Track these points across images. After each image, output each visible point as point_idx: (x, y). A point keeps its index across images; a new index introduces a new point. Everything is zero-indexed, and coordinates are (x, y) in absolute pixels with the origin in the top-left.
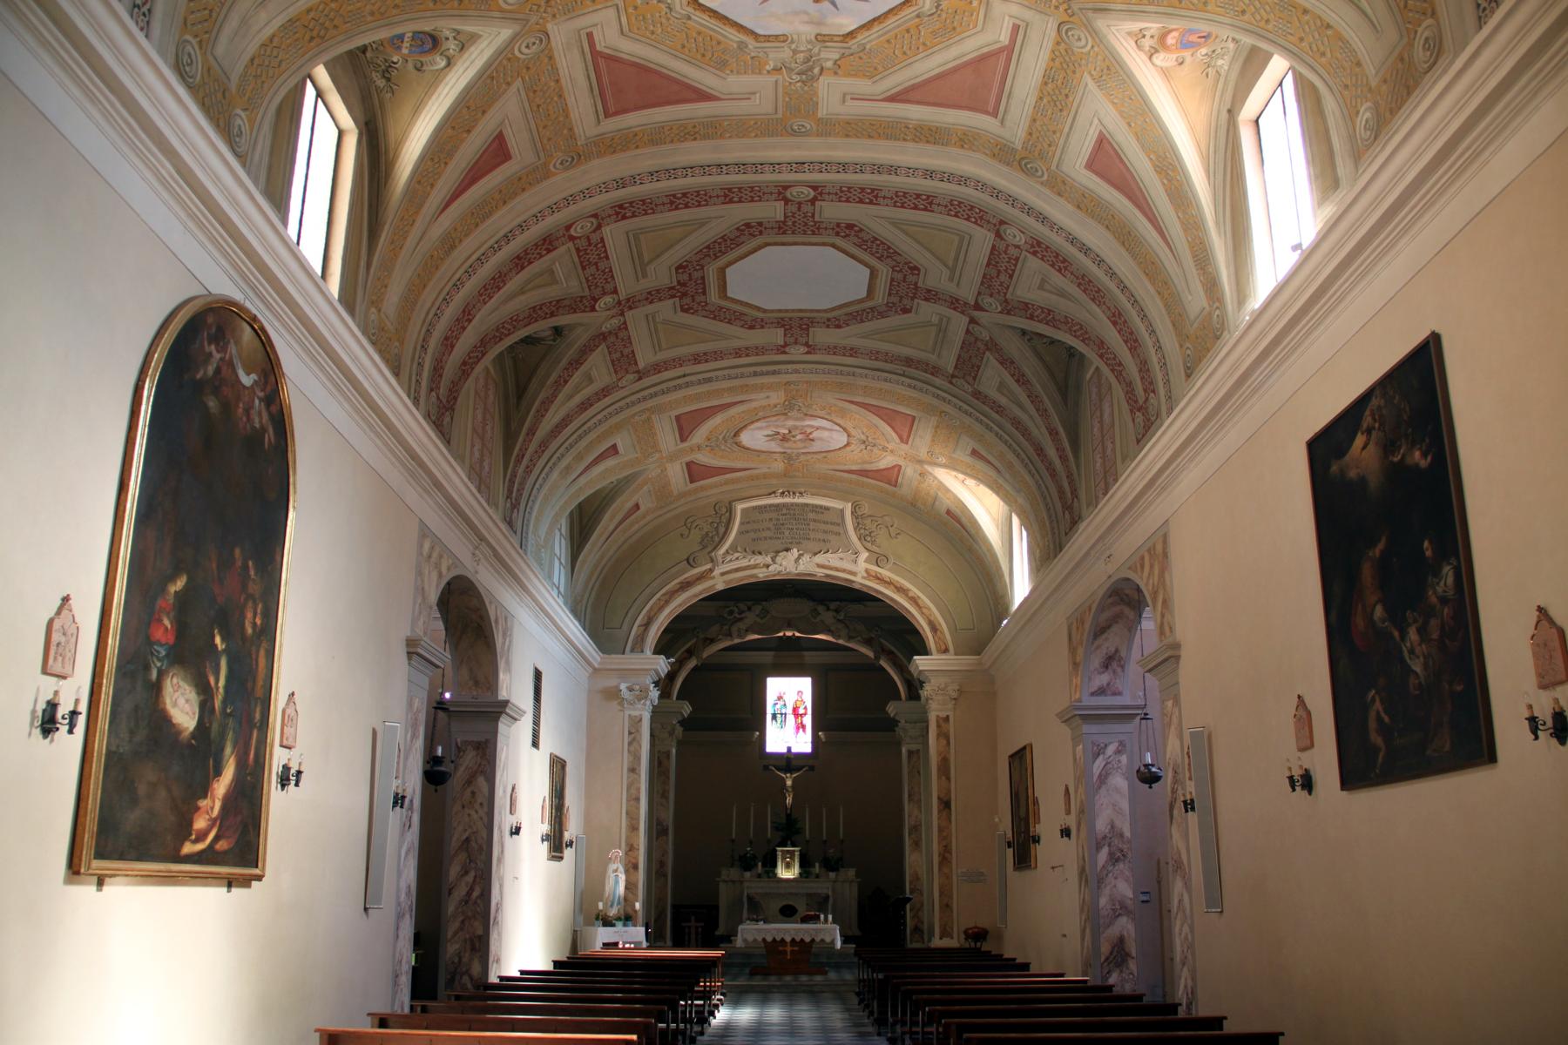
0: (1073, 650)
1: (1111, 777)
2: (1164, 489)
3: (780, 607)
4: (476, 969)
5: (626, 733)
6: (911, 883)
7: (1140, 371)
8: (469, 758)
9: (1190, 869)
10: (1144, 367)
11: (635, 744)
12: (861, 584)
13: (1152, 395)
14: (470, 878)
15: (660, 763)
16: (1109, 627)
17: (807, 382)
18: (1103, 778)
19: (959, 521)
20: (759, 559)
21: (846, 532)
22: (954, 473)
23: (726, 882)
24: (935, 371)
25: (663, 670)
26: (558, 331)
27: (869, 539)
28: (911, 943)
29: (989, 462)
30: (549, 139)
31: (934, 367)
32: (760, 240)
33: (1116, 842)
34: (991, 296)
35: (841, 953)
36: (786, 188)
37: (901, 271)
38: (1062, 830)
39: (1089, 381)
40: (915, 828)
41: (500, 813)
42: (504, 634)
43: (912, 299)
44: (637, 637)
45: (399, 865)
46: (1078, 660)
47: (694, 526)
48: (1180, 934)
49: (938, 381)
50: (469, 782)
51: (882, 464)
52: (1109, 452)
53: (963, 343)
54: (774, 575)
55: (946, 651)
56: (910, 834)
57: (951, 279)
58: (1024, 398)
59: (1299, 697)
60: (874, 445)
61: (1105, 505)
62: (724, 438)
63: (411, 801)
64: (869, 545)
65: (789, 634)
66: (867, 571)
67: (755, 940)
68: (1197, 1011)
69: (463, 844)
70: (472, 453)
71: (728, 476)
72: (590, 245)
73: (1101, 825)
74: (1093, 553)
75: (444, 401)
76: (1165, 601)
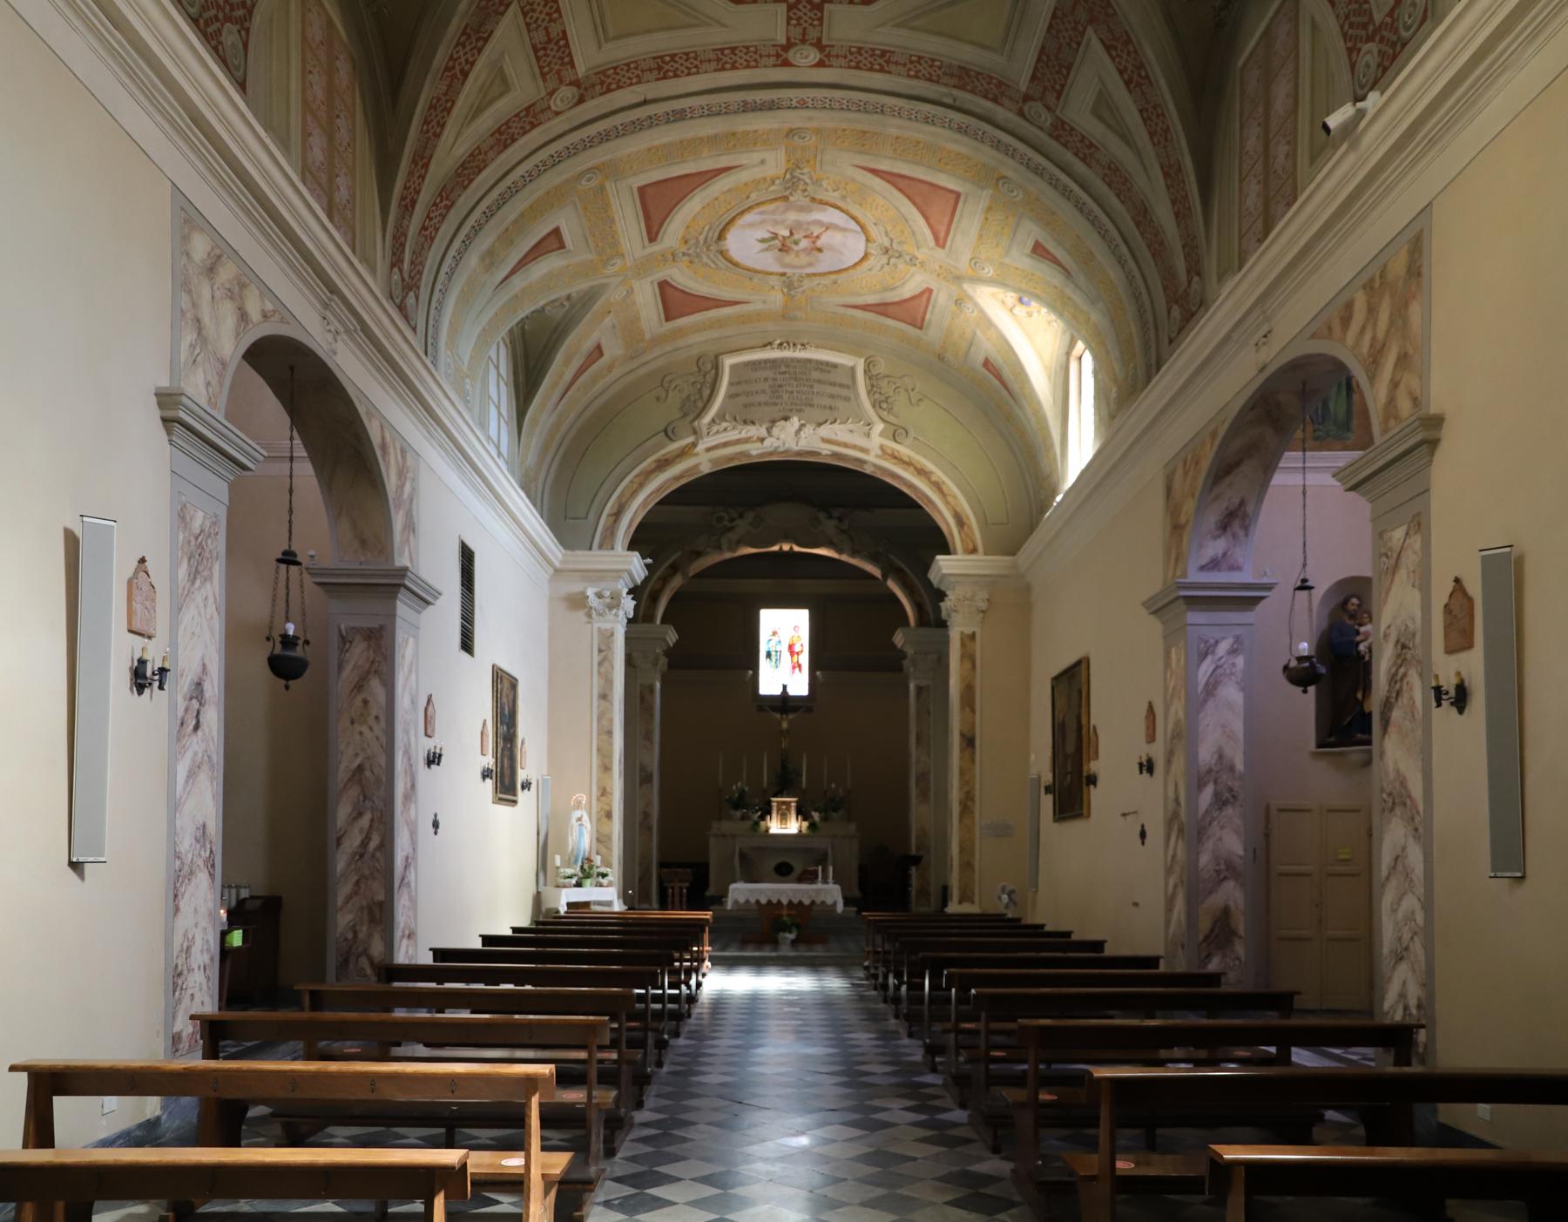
2: (1432, 142)
4: (377, 948)
8: (358, 653)
11: (606, 664)
12: (875, 466)
14: (365, 821)
16: (1238, 464)
18: (1211, 688)
19: (999, 377)
21: (857, 396)
23: (717, 836)
25: (639, 575)
27: (884, 406)
33: (1225, 777)
38: (1141, 765)
40: (923, 777)
41: (407, 732)
42: (402, 474)
44: (606, 529)
46: (1183, 519)
47: (673, 386)
48: (1394, 911)
50: (359, 686)
51: (908, 290)
53: (1054, 16)
54: (771, 454)
55: (974, 551)
58: (1133, 118)
59: (1457, 580)
60: (900, 256)
64: (884, 414)
65: (786, 547)
66: (882, 448)
67: (747, 902)
69: (354, 775)
71: (712, 313)
73: (1206, 755)
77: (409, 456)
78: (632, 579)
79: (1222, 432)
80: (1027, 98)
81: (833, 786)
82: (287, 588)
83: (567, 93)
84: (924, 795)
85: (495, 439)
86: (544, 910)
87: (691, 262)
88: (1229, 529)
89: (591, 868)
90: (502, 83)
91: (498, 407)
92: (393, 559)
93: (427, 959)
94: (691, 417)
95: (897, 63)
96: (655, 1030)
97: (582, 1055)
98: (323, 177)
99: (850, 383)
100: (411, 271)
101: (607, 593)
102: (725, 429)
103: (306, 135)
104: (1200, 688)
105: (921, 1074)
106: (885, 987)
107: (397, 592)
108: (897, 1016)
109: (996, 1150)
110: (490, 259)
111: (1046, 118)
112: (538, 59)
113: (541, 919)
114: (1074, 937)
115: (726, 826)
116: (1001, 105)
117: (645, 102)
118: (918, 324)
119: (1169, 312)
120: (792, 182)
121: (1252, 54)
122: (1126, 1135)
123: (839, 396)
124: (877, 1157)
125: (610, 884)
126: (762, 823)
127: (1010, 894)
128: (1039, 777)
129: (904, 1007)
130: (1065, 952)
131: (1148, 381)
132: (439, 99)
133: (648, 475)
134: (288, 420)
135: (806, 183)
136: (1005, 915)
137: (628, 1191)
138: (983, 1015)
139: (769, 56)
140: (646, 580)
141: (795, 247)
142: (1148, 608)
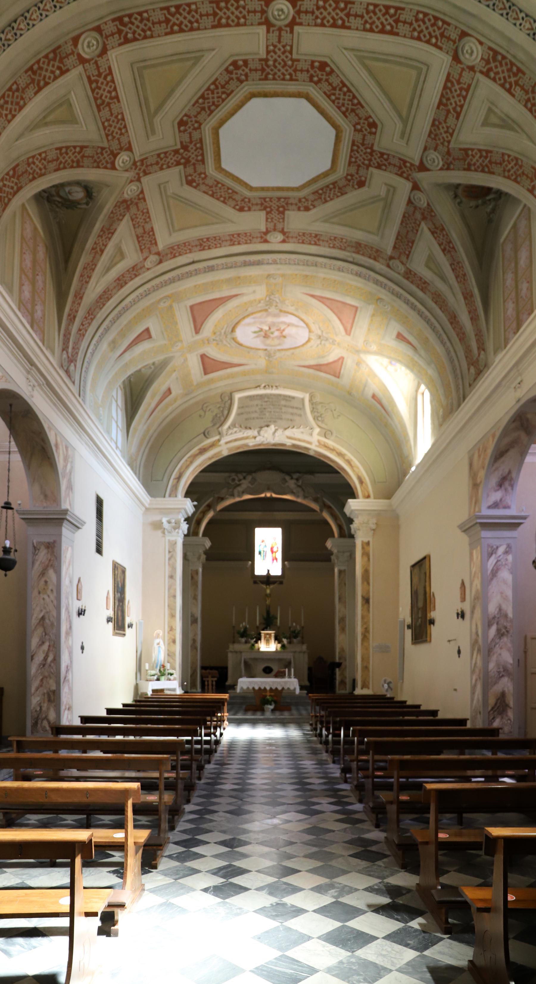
0: (473, 475)
1: (499, 572)
4: (52, 716)
5: (167, 552)
6: (339, 653)
8: (43, 555)
12: (316, 452)
14: (45, 647)
16: (507, 451)
17: (283, 276)
18: (495, 572)
20: (249, 433)
21: (305, 414)
23: (231, 652)
27: (320, 419)
29: (410, 343)
34: (435, 149)
35: (299, 697)
37: (361, 131)
38: (458, 614)
41: (67, 598)
42: (66, 459)
46: (478, 481)
47: (208, 409)
50: (43, 573)
51: (331, 358)
53: (404, 216)
54: (260, 445)
55: (368, 497)
56: (339, 623)
60: (327, 339)
62: (225, 333)
64: (320, 423)
65: (268, 495)
66: (319, 441)
67: (248, 688)
71: (229, 371)
73: (492, 609)
74: (504, 383)
77: (69, 449)
78: (187, 513)
79: (498, 434)
80: (391, 258)
81: (294, 624)
82: (6, 521)
83: (153, 258)
84: (343, 629)
85: (115, 439)
86: (140, 693)
87: (218, 344)
89: (164, 670)
90: (120, 254)
91: (117, 422)
92: (60, 505)
93: (77, 722)
94: (218, 425)
95: (323, 241)
96: (197, 760)
97: (156, 774)
98: (29, 306)
99: (301, 407)
100: (72, 352)
101: (173, 521)
102: (236, 432)
103: (21, 285)
104: (489, 572)
105: (339, 784)
106: (320, 735)
107: (62, 523)
108: (327, 752)
109: (377, 826)
111: (402, 269)
112: (139, 242)
113: (138, 699)
114: (422, 708)
115: (237, 647)
116: (378, 261)
117: (193, 262)
118: (337, 375)
119: (469, 369)
120: (270, 302)
121: (507, 237)
122: (447, 818)
123: (296, 414)
124: (314, 830)
125: (175, 679)
126: (256, 645)
127: (389, 684)
128: (404, 621)
129: (330, 745)
130: (417, 716)
131: (459, 405)
132: (88, 264)
133: (195, 456)
134: (7, 432)
135: (277, 303)
136: (385, 695)
137: (181, 849)
138: (371, 752)
139: (257, 237)
140: (194, 514)
141: (272, 336)
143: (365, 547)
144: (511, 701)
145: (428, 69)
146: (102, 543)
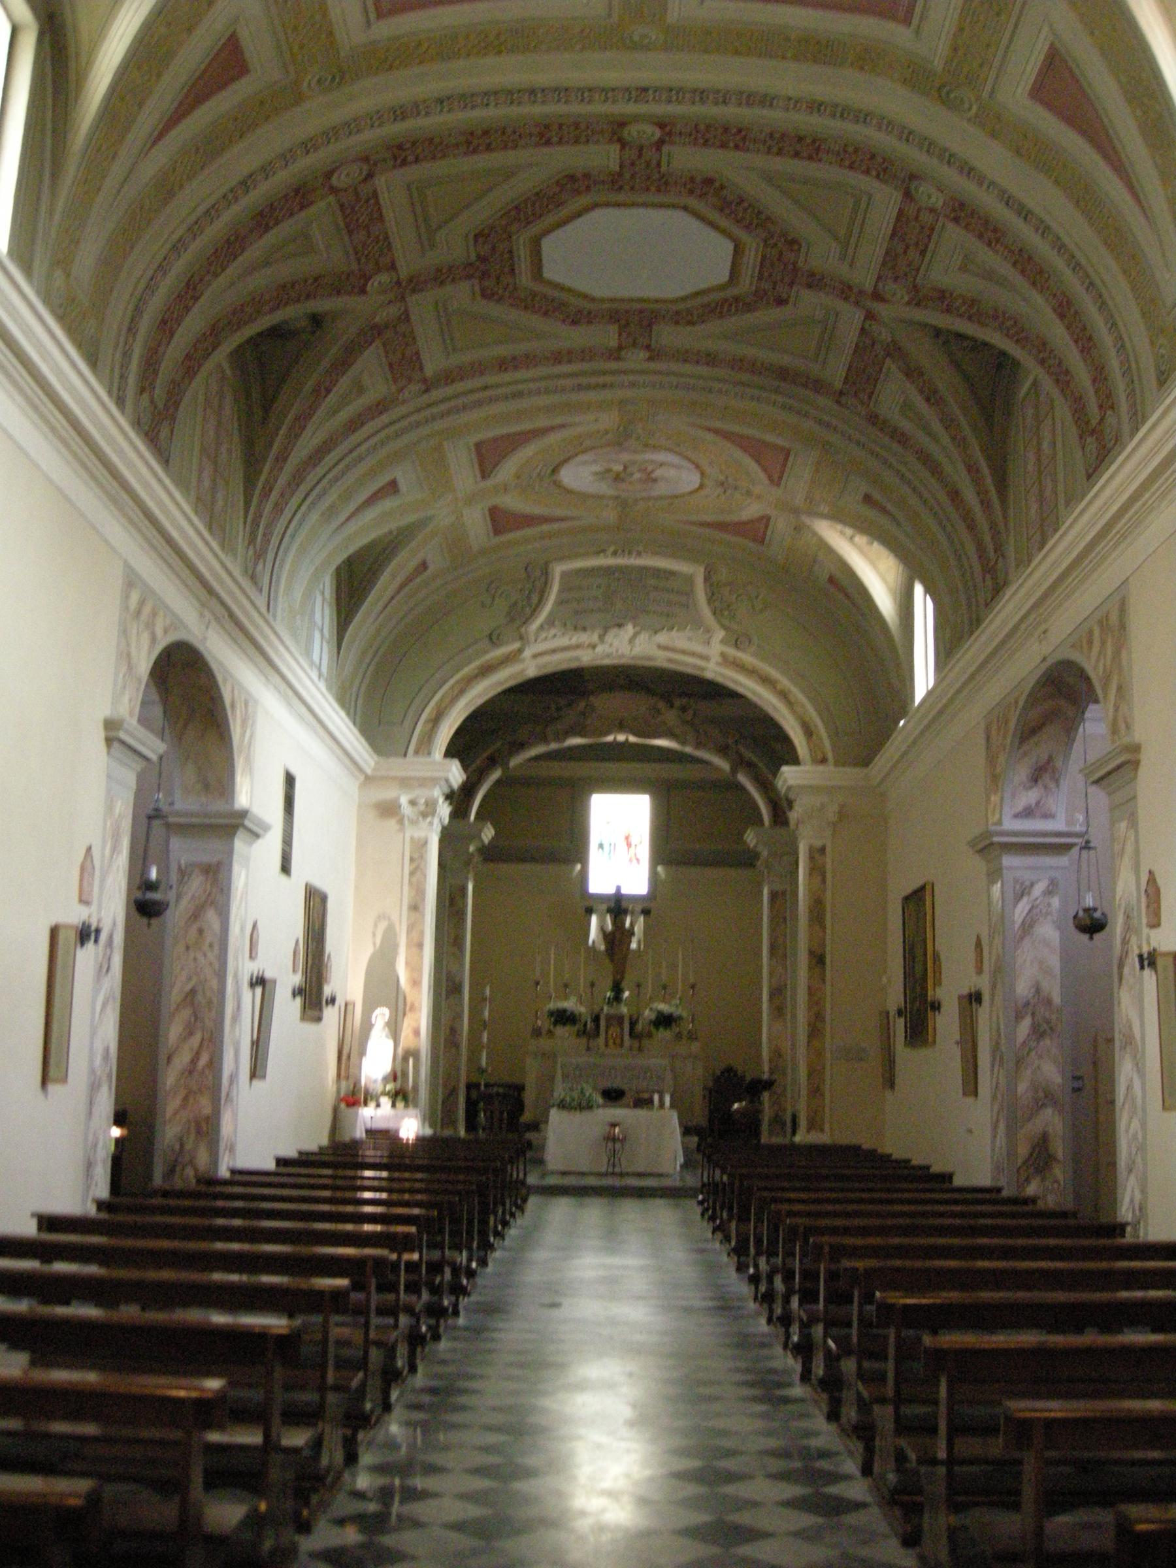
0: (991, 760)
2: (1124, 537)
3: (606, 703)
7: (1094, 381)
8: (196, 884)
9: (1143, 1043)
10: (1100, 375)
11: (418, 874)
13: (1109, 412)
14: (196, 1040)
15: (452, 901)
18: (1028, 926)
20: (584, 638)
22: (839, 527)
24: (818, 386)
26: (317, 320)
27: (726, 613)
28: (771, 1133)
30: (301, 47)
31: (817, 381)
32: (584, 200)
34: (896, 279)
36: (622, 124)
39: (1024, 400)
41: (236, 958)
43: (791, 284)
45: (93, 1018)
48: (1127, 1131)
49: (822, 401)
50: (196, 915)
52: (1048, 493)
55: (824, 761)
57: (842, 258)
58: (937, 426)
60: (736, 488)
61: (1040, 563)
62: (539, 475)
63: (111, 937)
65: (621, 738)
68: (1146, 1234)
70: (200, 480)
71: (545, 527)
72: (358, 199)
73: (1023, 988)
75: (161, 406)
76: (1120, 688)
78: (450, 786)
80: (841, 393)
88: (1040, 782)
91: (322, 631)
97: (251, 1437)
101: (422, 801)
102: (555, 636)
110: (332, 511)
133: (470, 681)
142: (973, 847)
143: (817, 856)
144: (1059, 1148)
145: (870, 199)
146: (290, 854)
